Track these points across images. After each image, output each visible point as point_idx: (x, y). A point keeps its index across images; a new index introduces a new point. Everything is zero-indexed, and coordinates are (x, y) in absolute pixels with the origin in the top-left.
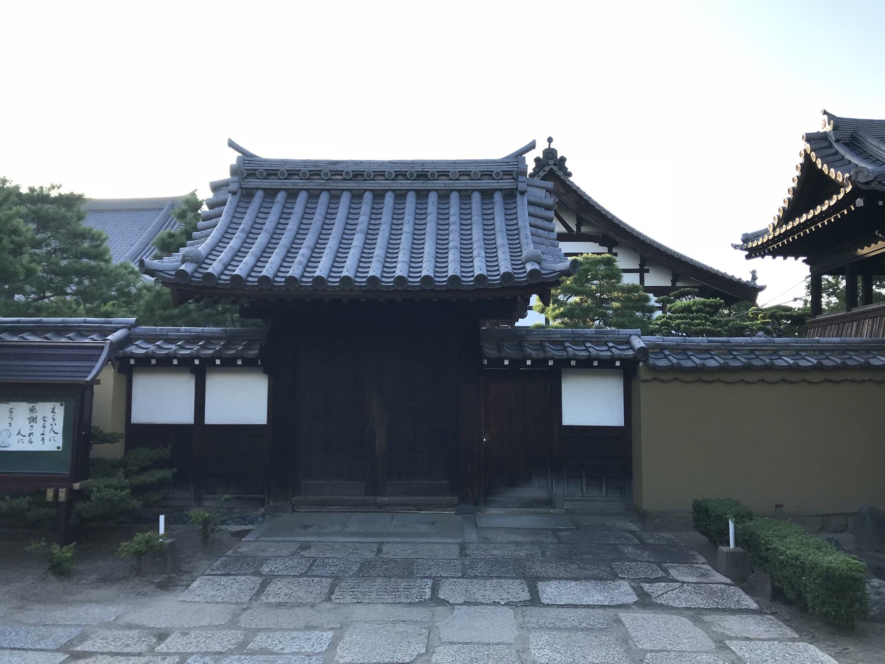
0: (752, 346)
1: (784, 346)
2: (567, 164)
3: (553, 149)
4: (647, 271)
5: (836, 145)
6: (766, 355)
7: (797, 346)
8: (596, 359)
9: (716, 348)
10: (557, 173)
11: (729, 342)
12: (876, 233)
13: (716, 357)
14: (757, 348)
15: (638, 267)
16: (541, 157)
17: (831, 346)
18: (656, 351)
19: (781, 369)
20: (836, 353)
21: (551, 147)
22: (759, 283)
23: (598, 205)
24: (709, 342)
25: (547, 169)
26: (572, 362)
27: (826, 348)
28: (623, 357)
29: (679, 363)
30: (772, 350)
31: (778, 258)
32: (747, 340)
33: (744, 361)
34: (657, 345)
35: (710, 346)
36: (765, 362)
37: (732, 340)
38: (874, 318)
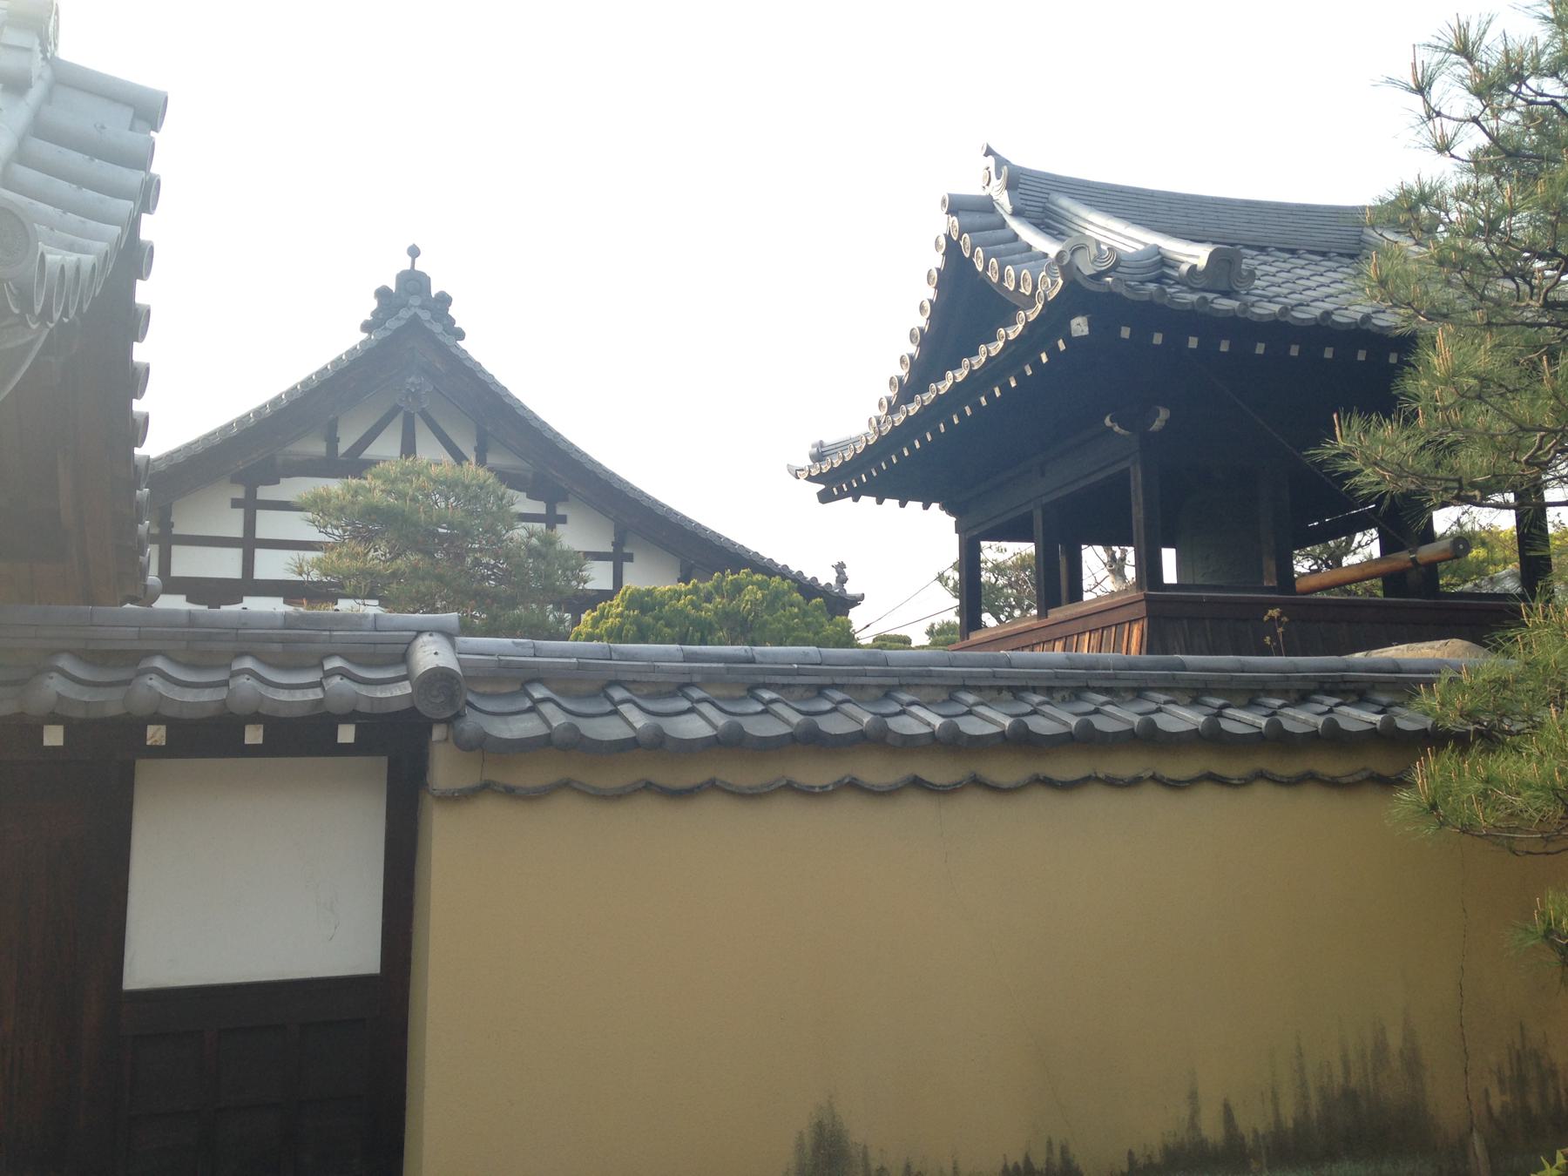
0: (817, 674)
1: (914, 675)
2: (452, 311)
3: (422, 275)
4: (630, 558)
5: (1015, 225)
6: (863, 702)
7: (954, 675)
8: (256, 718)
9: (710, 679)
10: (428, 325)
11: (752, 660)
12: (1108, 421)
13: (706, 708)
14: (838, 680)
15: (610, 549)
16: (393, 287)
17: (1048, 677)
18: (506, 689)
19: (910, 745)
20: (1058, 696)
21: (417, 268)
22: (851, 589)
23: (523, 407)
24: (688, 658)
25: (405, 314)
26: (151, 730)
27: (1031, 683)
28: (363, 707)
29: (574, 728)
30: (879, 686)
31: (887, 501)
32: (806, 654)
33: (796, 718)
34: (508, 666)
35: (691, 672)
36: (860, 722)
37: (763, 654)
38: (1103, 628)
